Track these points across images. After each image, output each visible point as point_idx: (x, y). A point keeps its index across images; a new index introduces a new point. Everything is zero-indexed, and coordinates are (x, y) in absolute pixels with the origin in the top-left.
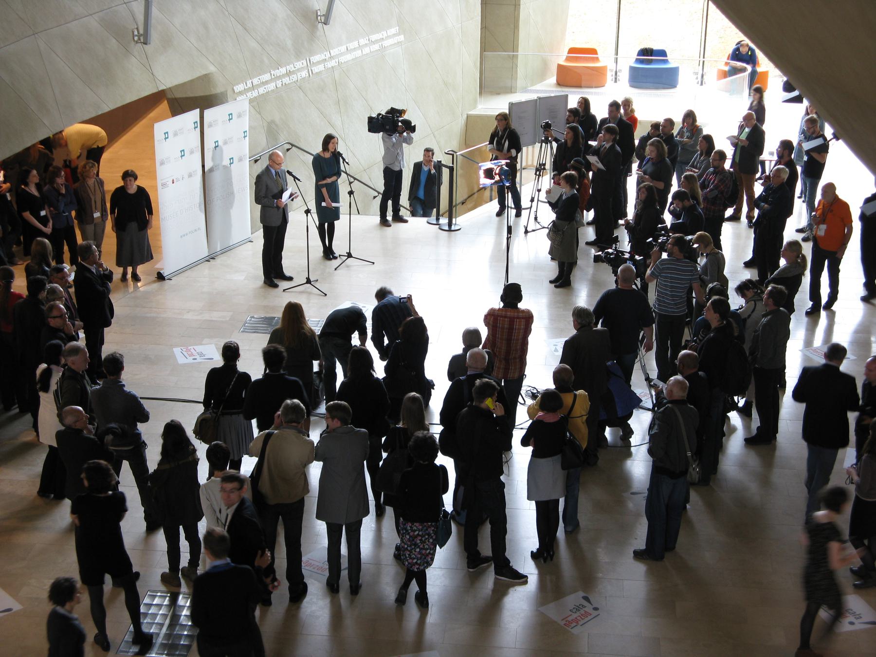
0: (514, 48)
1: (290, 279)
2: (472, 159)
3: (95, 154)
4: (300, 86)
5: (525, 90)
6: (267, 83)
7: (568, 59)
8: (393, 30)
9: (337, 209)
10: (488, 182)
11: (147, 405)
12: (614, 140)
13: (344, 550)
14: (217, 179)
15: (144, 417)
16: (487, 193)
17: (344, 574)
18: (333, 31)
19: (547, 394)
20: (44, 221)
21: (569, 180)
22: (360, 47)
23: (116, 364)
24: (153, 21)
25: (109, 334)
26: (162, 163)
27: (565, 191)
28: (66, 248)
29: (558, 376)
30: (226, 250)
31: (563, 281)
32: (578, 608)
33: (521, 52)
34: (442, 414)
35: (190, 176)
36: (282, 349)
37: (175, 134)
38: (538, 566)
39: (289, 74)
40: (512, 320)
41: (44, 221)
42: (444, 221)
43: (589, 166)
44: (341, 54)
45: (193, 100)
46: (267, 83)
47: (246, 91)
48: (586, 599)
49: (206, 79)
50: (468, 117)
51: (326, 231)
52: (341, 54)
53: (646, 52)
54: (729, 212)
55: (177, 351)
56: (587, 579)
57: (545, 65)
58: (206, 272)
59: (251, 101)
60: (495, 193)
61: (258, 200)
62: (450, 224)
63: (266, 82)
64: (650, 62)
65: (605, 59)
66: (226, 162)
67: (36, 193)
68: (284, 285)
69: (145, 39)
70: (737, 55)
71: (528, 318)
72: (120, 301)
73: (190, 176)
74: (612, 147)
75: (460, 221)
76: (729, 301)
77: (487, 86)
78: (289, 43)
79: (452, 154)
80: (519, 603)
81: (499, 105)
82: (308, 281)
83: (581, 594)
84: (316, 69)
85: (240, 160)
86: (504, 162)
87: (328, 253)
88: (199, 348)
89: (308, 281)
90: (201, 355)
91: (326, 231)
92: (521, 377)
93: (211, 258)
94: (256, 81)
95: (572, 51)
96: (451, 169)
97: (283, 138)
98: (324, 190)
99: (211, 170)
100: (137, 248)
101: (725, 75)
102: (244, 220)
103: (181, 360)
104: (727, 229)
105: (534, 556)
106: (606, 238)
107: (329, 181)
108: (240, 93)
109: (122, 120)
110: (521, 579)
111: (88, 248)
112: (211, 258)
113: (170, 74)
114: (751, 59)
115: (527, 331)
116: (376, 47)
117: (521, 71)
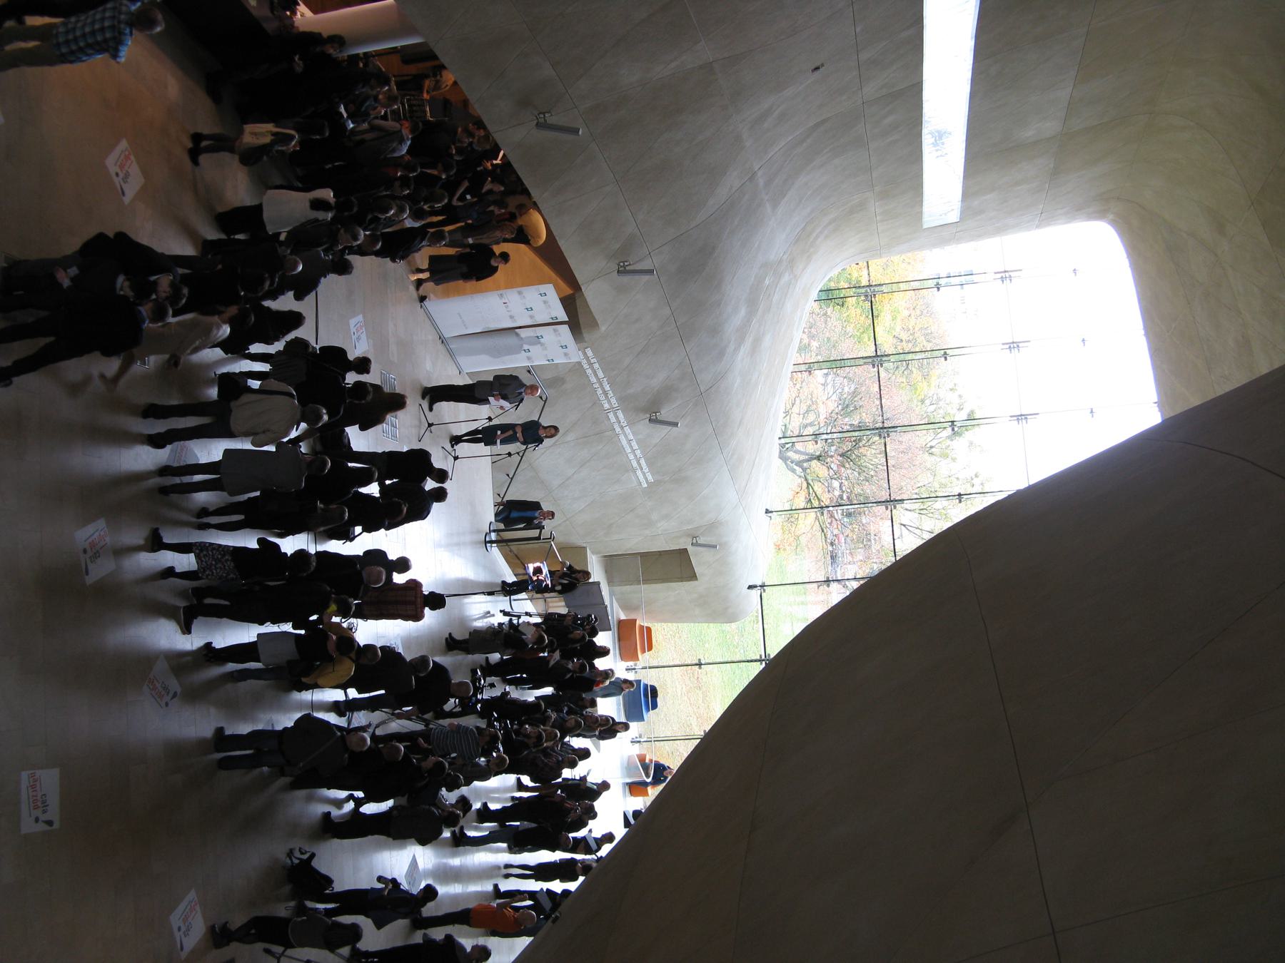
0: (646, 581)
1: (431, 409)
2: (548, 555)
3: (522, 237)
4: (596, 403)
5: (612, 594)
6: (596, 375)
7: (642, 627)
8: (650, 478)
9: (495, 443)
10: (531, 570)
11: (310, 298)
12: (574, 672)
13: (198, 478)
14: (510, 340)
15: (299, 297)
16: (521, 571)
17: (177, 480)
18: (644, 427)
19: (351, 641)
20: (462, 198)
21: (541, 639)
22: (633, 451)
23: (343, 268)
24: (637, 277)
25: (370, 260)
26: (520, 293)
27: (529, 635)
28: (440, 218)
29: (370, 648)
30: (451, 354)
31: (452, 644)
32: (166, 689)
33: (643, 587)
34: (325, 553)
35: (511, 317)
36: (370, 398)
37: (545, 302)
38: (200, 649)
39: (605, 393)
40: (414, 603)
41: (462, 198)
42: (493, 536)
43: (552, 651)
44: (626, 436)
45: (576, 316)
46: (596, 375)
47: (587, 358)
48: (175, 695)
49: (594, 324)
50: (585, 548)
51: (475, 436)
52: (626, 436)
53: (654, 691)
54: (526, 780)
55: (360, 318)
56: (194, 695)
57: (635, 608)
58: (430, 337)
59: (579, 363)
60: (522, 578)
61: (496, 377)
62: (491, 542)
63: (596, 374)
64: (646, 695)
65: (645, 658)
66: (526, 347)
67: (484, 190)
68: (425, 404)
69: (622, 271)
70: (660, 770)
71: (417, 617)
72: (396, 269)
73: (511, 317)
74: (569, 671)
75: (495, 550)
76: (383, 530)
77: (612, 563)
78: (631, 391)
79: (551, 538)
80: (167, 637)
81: (597, 574)
82: (430, 425)
83: (179, 690)
84: (611, 416)
85: (529, 358)
86: (549, 582)
87: (456, 440)
88: (364, 337)
89: (430, 425)
90: (359, 339)
91: (475, 436)
92: (365, 616)
93: (443, 340)
94: (596, 366)
95: (649, 630)
96: (538, 538)
97: (549, 393)
98: (511, 432)
99: (517, 335)
100: (442, 272)
101: (642, 759)
102: (481, 365)
103: (353, 322)
104: (511, 779)
105: (208, 645)
106: (489, 670)
107: (519, 435)
108: (585, 354)
109: (553, 257)
110: (187, 629)
111: (443, 238)
112: (443, 340)
113: (595, 294)
114: (656, 781)
115: (406, 618)
116: (635, 464)
117: (627, 588)
